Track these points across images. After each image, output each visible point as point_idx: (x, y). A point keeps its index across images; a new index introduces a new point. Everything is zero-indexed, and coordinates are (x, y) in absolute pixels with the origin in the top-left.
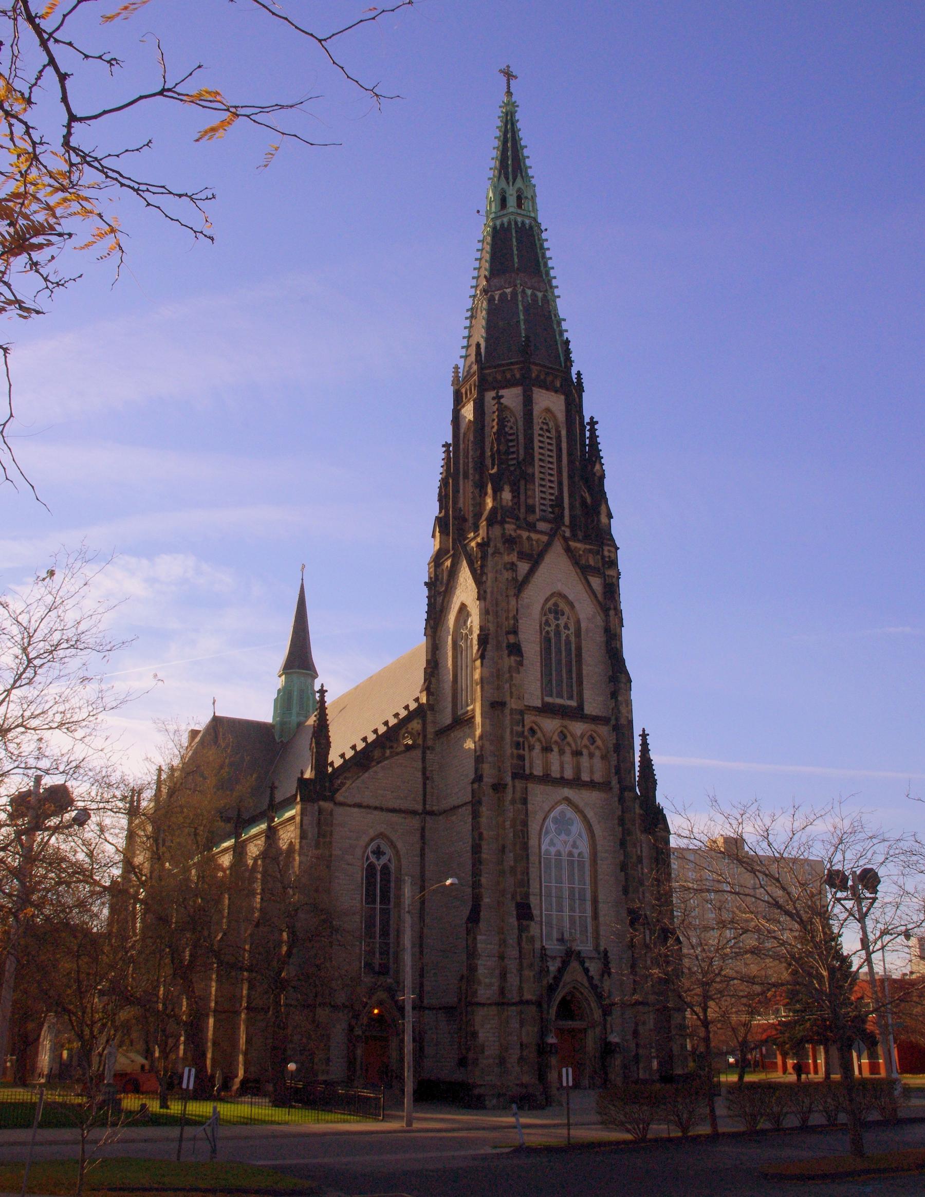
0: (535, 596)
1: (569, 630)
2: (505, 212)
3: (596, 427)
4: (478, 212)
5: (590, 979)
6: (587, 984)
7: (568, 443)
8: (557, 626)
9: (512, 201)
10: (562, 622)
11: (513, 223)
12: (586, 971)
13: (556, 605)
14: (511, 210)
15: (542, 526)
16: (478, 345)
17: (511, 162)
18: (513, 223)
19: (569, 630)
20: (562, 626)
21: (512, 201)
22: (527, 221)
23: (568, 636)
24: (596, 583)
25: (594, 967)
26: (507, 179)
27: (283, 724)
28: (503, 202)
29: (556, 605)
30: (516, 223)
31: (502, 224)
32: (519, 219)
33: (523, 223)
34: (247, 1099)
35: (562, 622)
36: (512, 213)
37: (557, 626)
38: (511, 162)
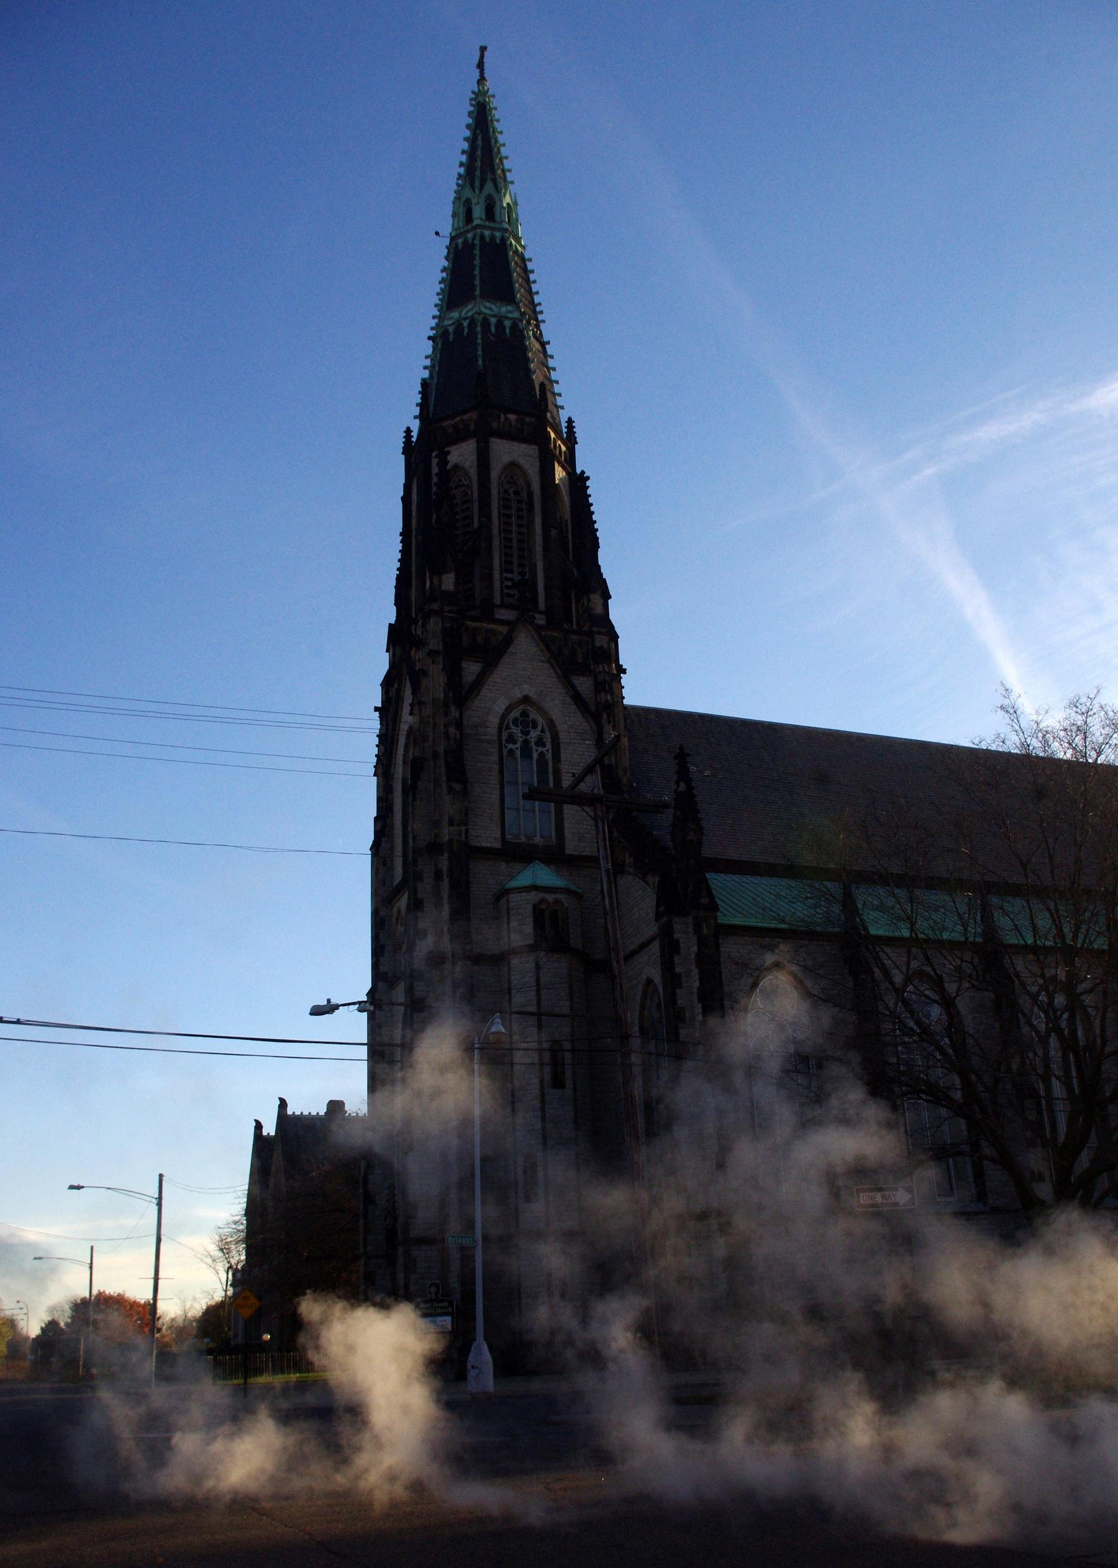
0: (493, 702)
1: (544, 746)
2: (470, 227)
3: (588, 483)
4: (437, 233)
7: (546, 596)
8: (526, 743)
9: (478, 212)
10: (534, 734)
11: (477, 184)
13: (524, 714)
14: (476, 222)
15: (503, 614)
16: (408, 431)
17: (483, 162)
18: (477, 184)
19: (544, 746)
20: (533, 740)
21: (478, 212)
22: (498, 234)
23: (542, 755)
24: (584, 685)
26: (472, 185)
27: (344, 1119)
28: (469, 218)
29: (524, 714)
30: (485, 322)
31: (493, 237)
32: (487, 233)
33: (493, 237)
34: (311, 1355)
35: (534, 734)
36: (478, 226)
37: (526, 743)
38: (483, 162)
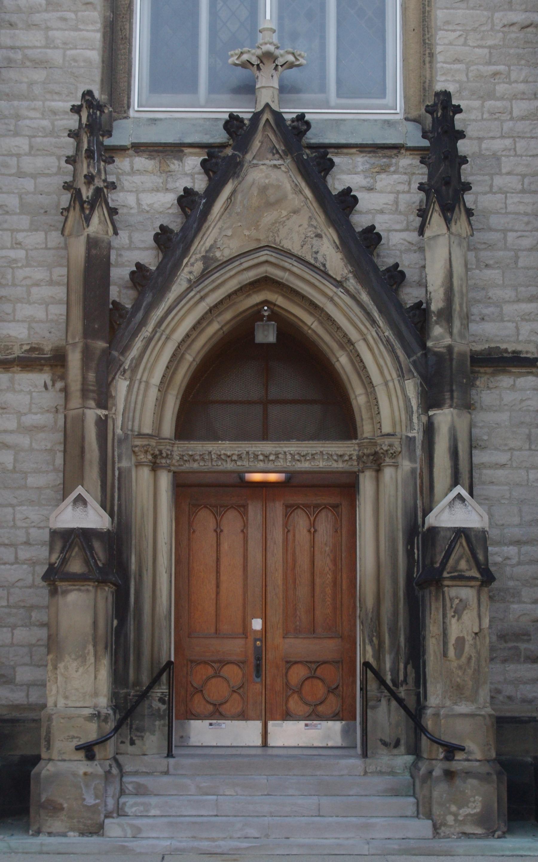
5: (362, 245)
6: (335, 261)
12: (340, 207)
25: (385, 197)
